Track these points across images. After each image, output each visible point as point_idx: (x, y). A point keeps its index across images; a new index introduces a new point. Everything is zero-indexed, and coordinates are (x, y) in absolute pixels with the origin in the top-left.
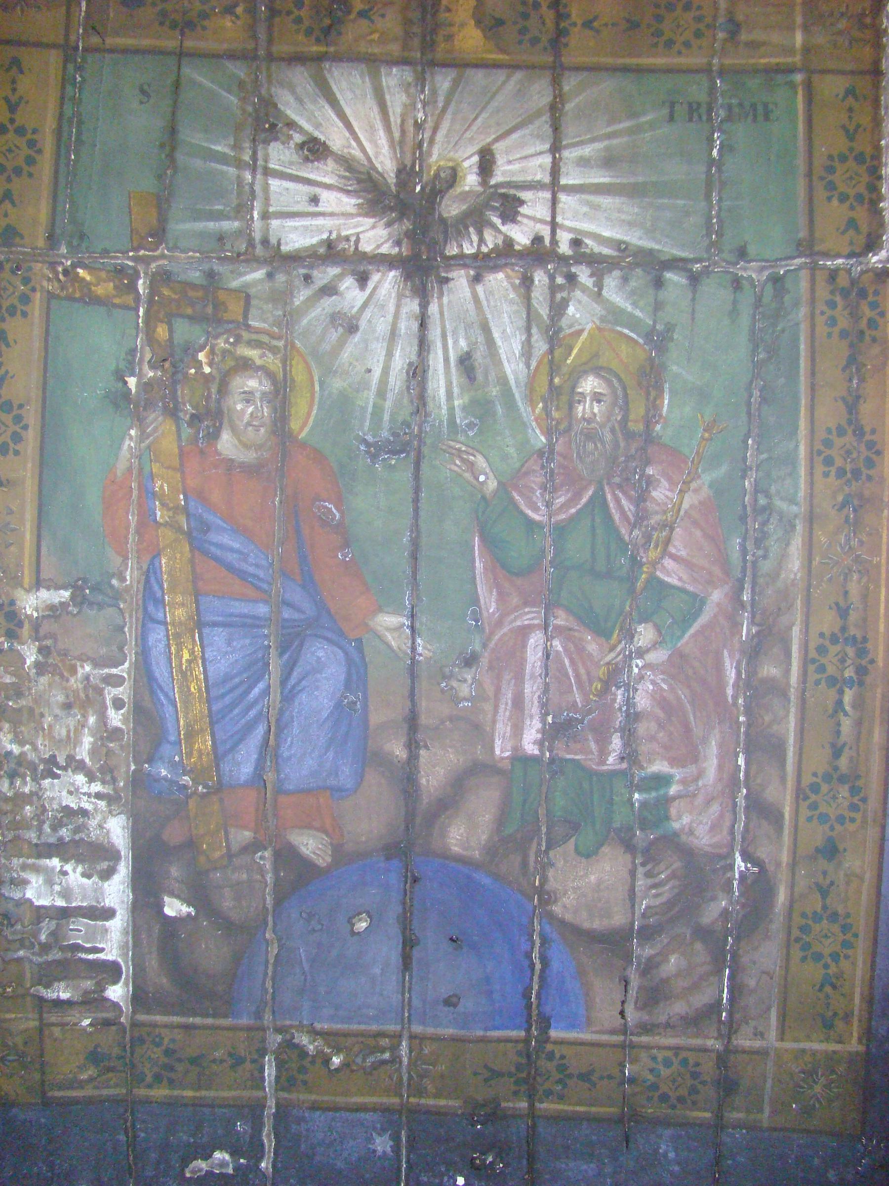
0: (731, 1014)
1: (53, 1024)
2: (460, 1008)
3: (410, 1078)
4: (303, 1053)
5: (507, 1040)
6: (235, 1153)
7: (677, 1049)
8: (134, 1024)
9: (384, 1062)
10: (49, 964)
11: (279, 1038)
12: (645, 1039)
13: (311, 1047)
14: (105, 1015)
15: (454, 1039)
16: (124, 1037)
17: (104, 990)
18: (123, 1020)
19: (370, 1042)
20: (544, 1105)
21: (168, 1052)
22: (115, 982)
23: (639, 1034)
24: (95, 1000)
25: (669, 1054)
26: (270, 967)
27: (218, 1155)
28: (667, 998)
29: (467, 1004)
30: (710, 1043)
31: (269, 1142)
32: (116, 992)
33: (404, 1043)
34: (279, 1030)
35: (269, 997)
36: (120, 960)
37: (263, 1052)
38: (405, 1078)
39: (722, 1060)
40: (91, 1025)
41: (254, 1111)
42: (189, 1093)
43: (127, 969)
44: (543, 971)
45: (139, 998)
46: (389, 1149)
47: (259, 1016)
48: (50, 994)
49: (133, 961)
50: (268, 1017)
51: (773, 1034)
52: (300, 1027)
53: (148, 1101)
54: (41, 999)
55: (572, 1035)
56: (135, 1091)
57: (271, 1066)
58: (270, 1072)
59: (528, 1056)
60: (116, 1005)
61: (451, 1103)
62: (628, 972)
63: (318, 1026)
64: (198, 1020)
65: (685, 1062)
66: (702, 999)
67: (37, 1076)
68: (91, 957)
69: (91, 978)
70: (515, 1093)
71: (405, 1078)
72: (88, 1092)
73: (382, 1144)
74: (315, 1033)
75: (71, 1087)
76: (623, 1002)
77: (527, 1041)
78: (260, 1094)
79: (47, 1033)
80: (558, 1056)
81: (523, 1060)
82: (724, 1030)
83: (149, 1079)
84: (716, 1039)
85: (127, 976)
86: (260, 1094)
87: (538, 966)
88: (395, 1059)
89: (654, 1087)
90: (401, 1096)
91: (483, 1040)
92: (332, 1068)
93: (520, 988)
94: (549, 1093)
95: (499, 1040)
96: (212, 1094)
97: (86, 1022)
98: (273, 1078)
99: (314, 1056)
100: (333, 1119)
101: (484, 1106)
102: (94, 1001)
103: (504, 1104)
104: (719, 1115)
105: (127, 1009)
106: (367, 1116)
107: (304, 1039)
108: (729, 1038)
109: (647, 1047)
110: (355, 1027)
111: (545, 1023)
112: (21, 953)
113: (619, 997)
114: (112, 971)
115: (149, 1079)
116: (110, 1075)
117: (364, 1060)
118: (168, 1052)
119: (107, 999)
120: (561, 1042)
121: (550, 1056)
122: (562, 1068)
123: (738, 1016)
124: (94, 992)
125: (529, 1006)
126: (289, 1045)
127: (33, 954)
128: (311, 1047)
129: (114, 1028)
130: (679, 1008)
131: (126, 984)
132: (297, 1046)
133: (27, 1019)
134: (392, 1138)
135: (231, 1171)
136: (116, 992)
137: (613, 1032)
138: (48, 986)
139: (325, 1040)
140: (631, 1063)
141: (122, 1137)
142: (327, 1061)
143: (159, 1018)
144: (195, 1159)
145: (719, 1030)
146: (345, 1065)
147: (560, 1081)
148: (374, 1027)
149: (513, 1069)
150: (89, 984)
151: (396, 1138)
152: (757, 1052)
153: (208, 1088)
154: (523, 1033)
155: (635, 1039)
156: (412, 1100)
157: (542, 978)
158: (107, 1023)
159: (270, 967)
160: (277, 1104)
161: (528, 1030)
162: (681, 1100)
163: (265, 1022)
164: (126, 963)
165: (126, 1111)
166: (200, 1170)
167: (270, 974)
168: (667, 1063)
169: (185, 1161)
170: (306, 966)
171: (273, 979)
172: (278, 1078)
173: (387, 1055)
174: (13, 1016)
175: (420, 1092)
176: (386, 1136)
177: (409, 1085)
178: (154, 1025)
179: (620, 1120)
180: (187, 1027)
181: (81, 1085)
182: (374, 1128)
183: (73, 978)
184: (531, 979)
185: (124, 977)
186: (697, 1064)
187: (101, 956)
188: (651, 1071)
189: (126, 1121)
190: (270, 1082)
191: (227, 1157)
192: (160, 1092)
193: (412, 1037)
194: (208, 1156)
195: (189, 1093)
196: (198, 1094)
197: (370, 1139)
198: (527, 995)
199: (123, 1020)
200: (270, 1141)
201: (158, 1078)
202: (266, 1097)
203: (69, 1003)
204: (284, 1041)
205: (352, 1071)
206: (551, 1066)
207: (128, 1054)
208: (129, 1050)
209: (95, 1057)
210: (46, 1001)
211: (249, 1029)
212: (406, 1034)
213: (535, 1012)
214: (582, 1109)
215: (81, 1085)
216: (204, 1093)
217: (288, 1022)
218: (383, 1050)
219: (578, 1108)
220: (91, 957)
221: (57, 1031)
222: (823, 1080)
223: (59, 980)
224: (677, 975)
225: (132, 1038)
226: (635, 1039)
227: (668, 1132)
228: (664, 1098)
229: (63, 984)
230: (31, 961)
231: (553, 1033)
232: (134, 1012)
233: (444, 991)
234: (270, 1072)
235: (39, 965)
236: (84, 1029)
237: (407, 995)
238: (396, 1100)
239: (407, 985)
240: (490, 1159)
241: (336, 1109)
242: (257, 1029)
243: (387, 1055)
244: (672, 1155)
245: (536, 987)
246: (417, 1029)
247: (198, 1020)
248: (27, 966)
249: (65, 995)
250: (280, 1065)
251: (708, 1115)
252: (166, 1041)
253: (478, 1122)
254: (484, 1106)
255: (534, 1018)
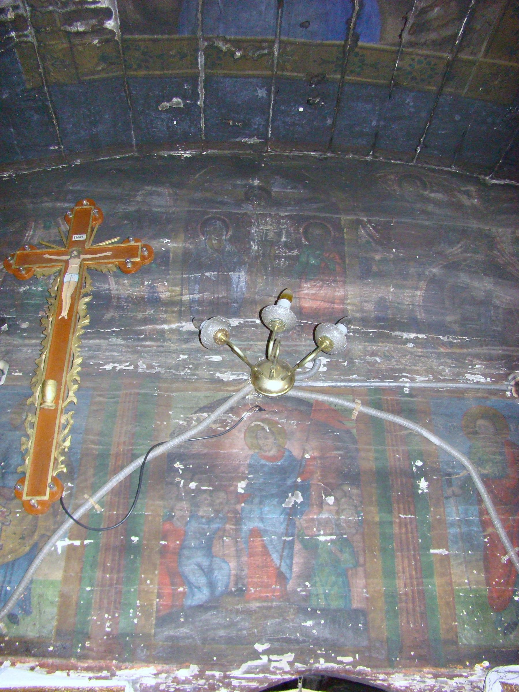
0: (460, 43)
1: (78, 45)
2: (309, 29)
3: (278, 62)
4: (219, 50)
5: (333, 46)
6: (184, 98)
7: (426, 57)
8: (123, 41)
9: (263, 55)
10: (68, 13)
11: (206, 44)
12: (410, 50)
13: (224, 48)
14: (106, 37)
15: (304, 44)
16: (118, 47)
17: (103, 24)
18: (116, 38)
19: (258, 45)
20: (349, 78)
21: (144, 54)
22: (109, 18)
23: (408, 47)
24: (99, 29)
25: (422, 58)
26: (200, 7)
27: (175, 100)
28: (429, 30)
29: (313, 27)
30: (445, 55)
31: (202, 93)
32: (110, 24)
33: (276, 46)
34: (205, 39)
35: (199, 22)
36: (110, 7)
37: (197, 50)
38: (275, 62)
39: (449, 65)
40: (99, 43)
41: (194, 79)
42: (158, 72)
43: (115, 12)
44: (359, 11)
45: (124, 26)
46: (265, 95)
47: (194, 32)
48: (72, 29)
49: (118, 6)
50: (199, 33)
51: (481, 54)
52: (218, 38)
53: (135, 77)
54: (68, 33)
55: (371, 45)
56: (128, 73)
57: (201, 57)
58: (201, 60)
59: (344, 52)
60: (111, 32)
61: (299, 75)
62: (409, 14)
63: (228, 37)
64: (160, 37)
65: (430, 63)
66: (446, 33)
67: (73, 71)
68: (92, 6)
69: (95, 18)
70: (335, 71)
71: (275, 62)
72: (103, 75)
73: (261, 93)
74: (225, 40)
75: (93, 74)
76: (402, 30)
77: (344, 46)
78: (197, 71)
79: (74, 49)
80: (360, 55)
81: (341, 56)
82: (455, 50)
83: (135, 66)
84: (449, 53)
85: (116, 15)
86: (197, 71)
87: (357, 8)
88: (271, 53)
89: (410, 73)
90: (273, 71)
91: (321, 45)
92: (236, 58)
93: (345, 20)
94: (352, 72)
95: (329, 45)
96: (170, 72)
97: (96, 42)
98: (203, 63)
99: (225, 52)
100: (236, 82)
101: (316, 76)
102: (99, 30)
103: (327, 76)
104: (441, 89)
105: (118, 33)
106: (255, 80)
107: (220, 44)
108: (456, 55)
109: (411, 54)
110: (249, 38)
111: (356, 39)
112: (51, 8)
113: (401, 28)
114: (107, 14)
115: (135, 66)
116: (113, 66)
117: (253, 54)
118: (144, 54)
119: (106, 29)
120: (362, 48)
121: (357, 54)
122: (362, 61)
123: (464, 43)
124: (98, 25)
125: (348, 29)
126: (211, 46)
127: (58, 8)
128: (224, 48)
129: (112, 43)
130: (433, 36)
131: (116, 20)
132: (217, 47)
133: (63, 44)
134: (266, 90)
135: (182, 106)
136: (110, 24)
137: (394, 45)
138: (71, 25)
139: (231, 44)
140: (400, 61)
141: (123, 94)
142: (233, 54)
143: (137, 37)
144: (164, 102)
145: (452, 49)
146: (243, 57)
147: (360, 67)
148: (260, 37)
149: (335, 60)
150: (94, 21)
151: (269, 91)
152: (470, 62)
153: (168, 69)
154: (343, 43)
155: (404, 49)
156: (278, 72)
157: (358, 15)
158: (107, 41)
159: (200, 7)
160: (205, 75)
161: (346, 40)
162: (422, 80)
163: (198, 36)
164: (114, 8)
165: (124, 82)
166: (167, 106)
167: (200, 10)
168: (420, 62)
169: (158, 102)
170: (221, 6)
171: (202, 13)
172: (205, 64)
173: (266, 51)
174: (54, 42)
175: (283, 69)
176: (264, 90)
177: (277, 66)
178: (135, 40)
179: (389, 87)
180: (154, 41)
181: (98, 72)
182: (258, 86)
183: (84, 20)
184: (352, 14)
185: (114, 16)
186: (435, 65)
187: (99, 5)
188: (410, 65)
189: (125, 87)
190: (201, 65)
191: (180, 100)
192: (141, 73)
193: (281, 42)
194: (170, 100)
195: (158, 72)
196: (162, 73)
197: (256, 91)
198: (348, 22)
199: (116, 38)
200: (202, 92)
201: (140, 67)
202: (199, 73)
203: (84, 33)
204: (208, 45)
205: (247, 59)
206: (356, 59)
207: (122, 55)
208: (121, 52)
209: (103, 58)
210: (71, 33)
211: (188, 39)
212: (277, 41)
213: (351, 32)
214: (369, 80)
215: (98, 72)
216: (166, 72)
217: (211, 36)
218: (264, 49)
219: (367, 80)
220: (92, 6)
221: (80, 48)
222: (500, 79)
223: (77, 22)
224: (437, 18)
225: (123, 47)
226: (404, 49)
227: (412, 94)
228: (414, 79)
229: (79, 23)
230: (58, 12)
231: (360, 43)
232: (122, 35)
233: (301, 20)
234: (201, 60)
235: (63, 14)
236: (95, 45)
237: (279, 21)
238: (270, 72)
239: (280, 15)
240: (318, 100)
241: (236, 77)
242: (193, 39)
243: (266, 51)
244: (411, 104)
245: (354, 19)
246: (284, 38)
247: (160, 37)
248: (56, 16)
249: (81, 29)
250: (207, 57)
251: (434, 88)
252: (142, 48)
253: (313, 84)
254: (316, 76)
255: (351, 35)
